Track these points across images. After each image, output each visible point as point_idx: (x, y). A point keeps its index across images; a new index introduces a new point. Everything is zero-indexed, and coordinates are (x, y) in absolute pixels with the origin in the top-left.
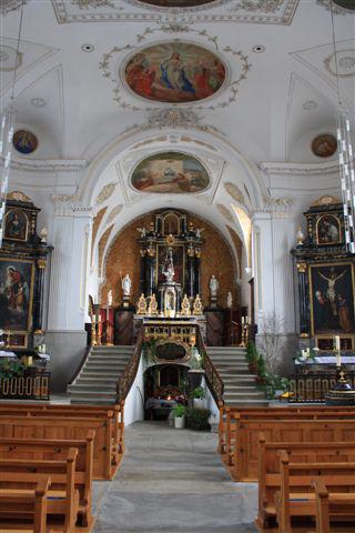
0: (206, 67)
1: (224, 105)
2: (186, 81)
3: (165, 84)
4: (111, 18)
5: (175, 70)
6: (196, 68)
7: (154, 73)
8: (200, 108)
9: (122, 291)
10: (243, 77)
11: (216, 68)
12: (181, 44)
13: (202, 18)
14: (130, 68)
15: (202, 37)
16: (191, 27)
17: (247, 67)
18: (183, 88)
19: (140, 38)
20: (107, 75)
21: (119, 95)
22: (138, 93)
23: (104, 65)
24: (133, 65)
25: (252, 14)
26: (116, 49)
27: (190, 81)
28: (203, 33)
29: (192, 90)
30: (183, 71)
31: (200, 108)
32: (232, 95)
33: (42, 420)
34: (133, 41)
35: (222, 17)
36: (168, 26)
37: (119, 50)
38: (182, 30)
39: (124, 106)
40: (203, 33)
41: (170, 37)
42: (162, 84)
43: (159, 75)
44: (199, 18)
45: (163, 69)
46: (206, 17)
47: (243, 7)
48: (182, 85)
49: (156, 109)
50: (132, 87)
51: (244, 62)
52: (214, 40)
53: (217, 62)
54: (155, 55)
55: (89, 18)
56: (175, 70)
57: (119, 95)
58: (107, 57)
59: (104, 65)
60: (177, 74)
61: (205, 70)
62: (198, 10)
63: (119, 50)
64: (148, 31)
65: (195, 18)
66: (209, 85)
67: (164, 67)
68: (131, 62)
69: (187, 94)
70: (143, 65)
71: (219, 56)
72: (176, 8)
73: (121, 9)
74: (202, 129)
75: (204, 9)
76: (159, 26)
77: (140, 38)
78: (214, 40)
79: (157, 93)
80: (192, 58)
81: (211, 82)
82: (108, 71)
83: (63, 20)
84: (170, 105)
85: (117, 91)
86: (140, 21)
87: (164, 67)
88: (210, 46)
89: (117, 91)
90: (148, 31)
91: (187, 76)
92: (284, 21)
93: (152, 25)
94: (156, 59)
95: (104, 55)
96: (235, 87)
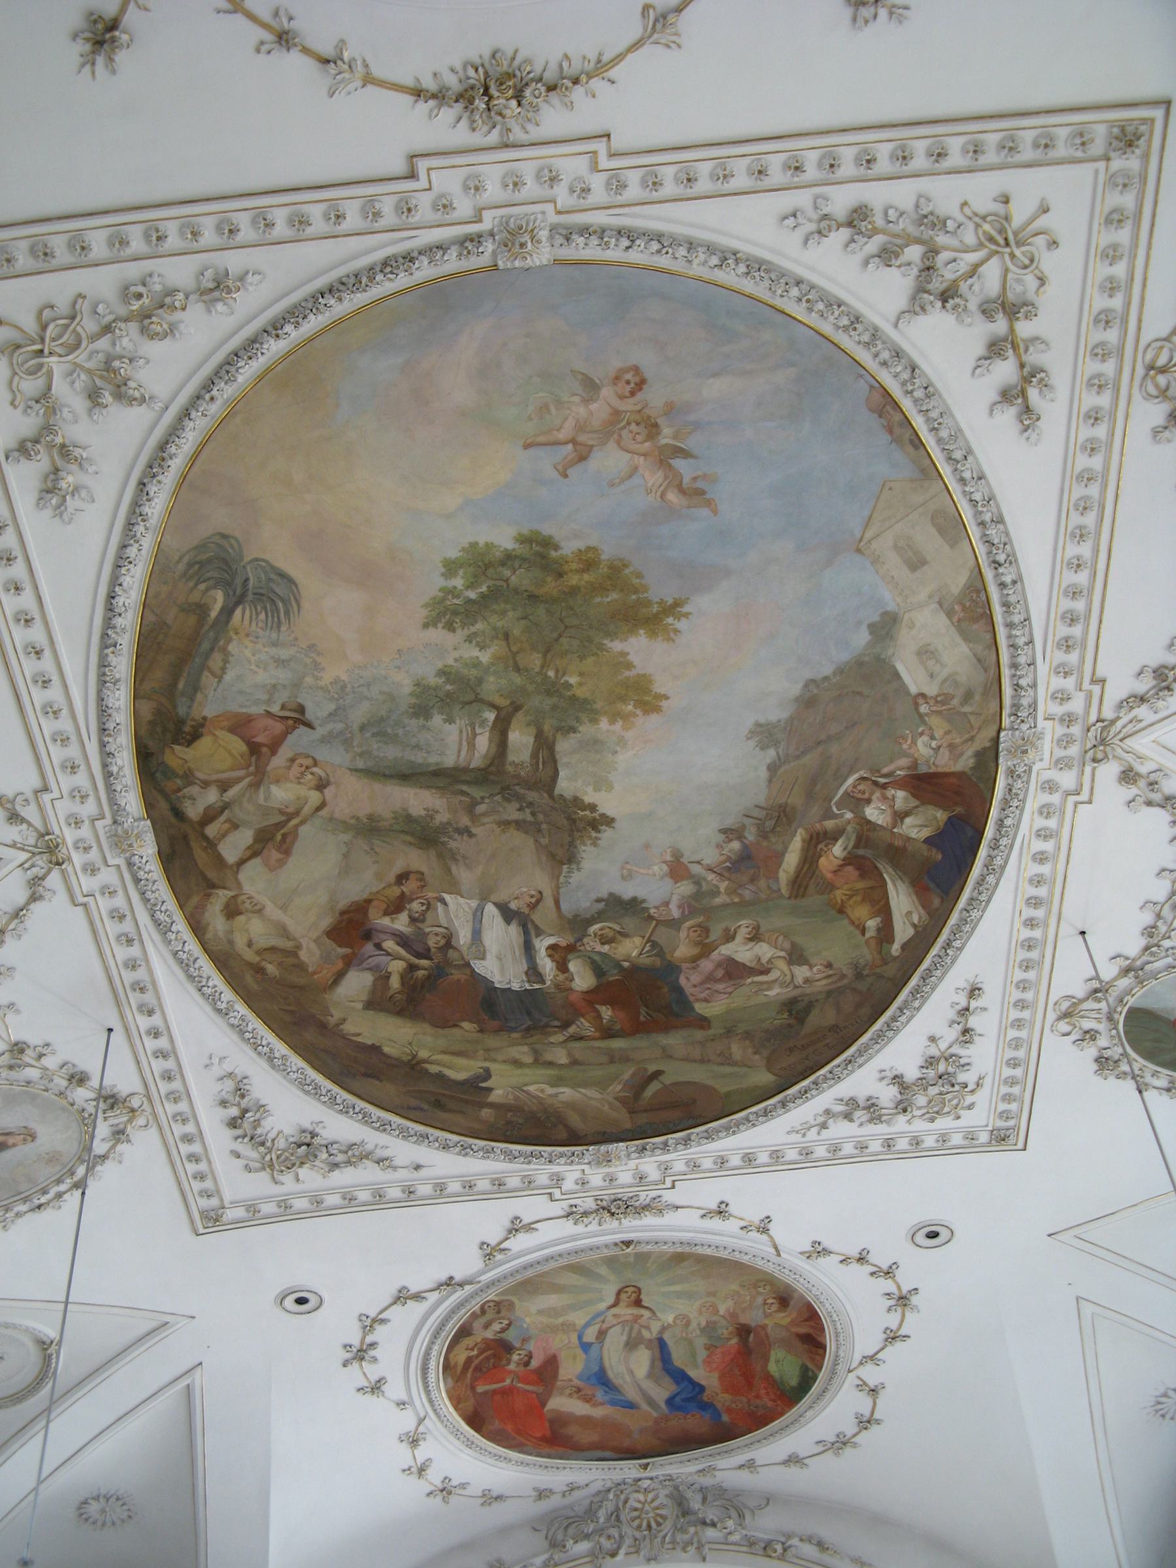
0: (745, 1319)
1: (841, 1443)
2: (680, 1377)
3: (600, 1395)
4: (379, 1199)
5: (631, 1345)
6: (709, 1329)
7: (552, 1363)
8: (750, 1465)
9: (483, 596)
10: (892, 1337)
11: (784, 1318)
12: (642, 1258)
13: (902, 1144)
14: (461, 1356)
15: (716, 1223)
16: (669, 1196)
17: (903, 1300)
18: (670, 1402)
19: (490, 1252)
20: (376, 1388)
21: (422, 1453)
22: (497, 1437)
23: (361, 1354)
24: (468, 1341)
25: (881, 1129)
26: (403, 1297)
27: (692, 1373)
28: (721, 1211)
29: (705, 1406)
30: (661, 1344)
31: (750, 1465)
32: (863, 1404)
33: (423, 1405)
34: (467, 1264)
35: (776, 1156)
36: (590, 1204)
37: (418, 1297)
38: (646, 1208)
39: (446, 1490)
40: (721, 1211)
41: (611, 1231)
42: (588, 1399)
43: (571, 1368)
44: (888, 1144)
45: (586, 1347)
46: (722, 1162)
47: (848, 1116)
48: (661, 1392)
49: (572, 1488)
50: (475, 1421)
51: (888, 1285)
52: (764, 1230)
53: (784, 1298)
54: (552, 1300)
55: (300, 1204)
56: (631, 1345)
57: (422, 1453)
58: (371, 1323)
59: (361, 1354)
60: (642, 1361)
61: (744, 1331)
62: (687, 1142)
63: (418, 1297)
64: (516, 1227)
65: (679, 1166)
66: (768, 1378)
67: (590, 1335)
68: (464, 1332)
69: (695, 1422)
70: (511, 1336)
71: (789, 1279)
72: (612, 1147)
73: (418, 1167)
74: (767, 1548)
75: (709, 1137)
76: (559, 1208)
77: (490, 1252)
78: (764, 1230)
79: (573, 1430)
80: (690, 1296)
81: (772, 1368)
82: (373, 1372)
83: (213, 1220)
84: (628, 1470)
85: (414, 1441)
86: (485, 1196)
87: (590, 1335)
88: (754, 1249)
89: (414, 1441)
90: (516, 1227)
91: (679, 1358)
92: (1000, 1138)
93: (531, 1207)
94: (553, 1312)
95: (362, 1317)
96: (871, 1374)
